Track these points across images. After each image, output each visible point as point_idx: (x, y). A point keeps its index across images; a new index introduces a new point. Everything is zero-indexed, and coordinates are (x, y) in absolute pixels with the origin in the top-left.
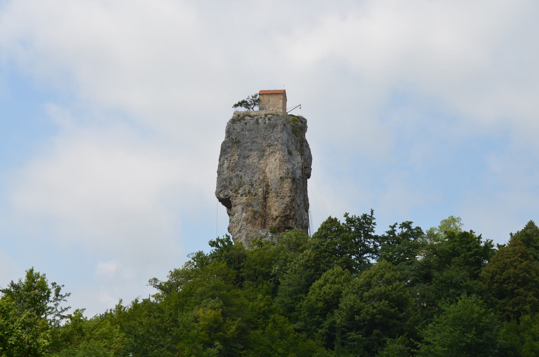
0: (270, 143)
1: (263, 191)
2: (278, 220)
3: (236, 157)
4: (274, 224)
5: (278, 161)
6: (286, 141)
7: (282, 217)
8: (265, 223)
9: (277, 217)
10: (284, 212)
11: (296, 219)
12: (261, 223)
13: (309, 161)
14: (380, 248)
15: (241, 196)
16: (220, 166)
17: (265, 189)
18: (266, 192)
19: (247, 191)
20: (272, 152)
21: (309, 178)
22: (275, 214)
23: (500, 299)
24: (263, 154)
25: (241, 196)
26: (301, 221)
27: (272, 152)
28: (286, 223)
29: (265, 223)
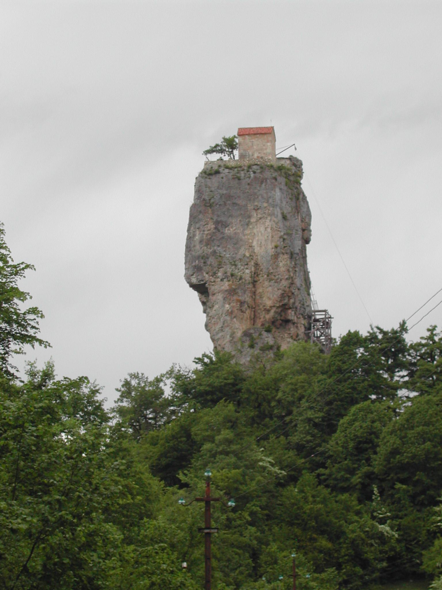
0: (257, 206)
4: (268, 317)
5: (269, 230)
6: (279, 202)
7: (278, 307)
8: (255, 315)
9: (271, 307)
12: (250, 317)
13: (307, 220)
16: (190, 239)
17: (253, 269)
20: (260, 219)
24: (249, 222)
25: (222, 280)
26: (302, 309)
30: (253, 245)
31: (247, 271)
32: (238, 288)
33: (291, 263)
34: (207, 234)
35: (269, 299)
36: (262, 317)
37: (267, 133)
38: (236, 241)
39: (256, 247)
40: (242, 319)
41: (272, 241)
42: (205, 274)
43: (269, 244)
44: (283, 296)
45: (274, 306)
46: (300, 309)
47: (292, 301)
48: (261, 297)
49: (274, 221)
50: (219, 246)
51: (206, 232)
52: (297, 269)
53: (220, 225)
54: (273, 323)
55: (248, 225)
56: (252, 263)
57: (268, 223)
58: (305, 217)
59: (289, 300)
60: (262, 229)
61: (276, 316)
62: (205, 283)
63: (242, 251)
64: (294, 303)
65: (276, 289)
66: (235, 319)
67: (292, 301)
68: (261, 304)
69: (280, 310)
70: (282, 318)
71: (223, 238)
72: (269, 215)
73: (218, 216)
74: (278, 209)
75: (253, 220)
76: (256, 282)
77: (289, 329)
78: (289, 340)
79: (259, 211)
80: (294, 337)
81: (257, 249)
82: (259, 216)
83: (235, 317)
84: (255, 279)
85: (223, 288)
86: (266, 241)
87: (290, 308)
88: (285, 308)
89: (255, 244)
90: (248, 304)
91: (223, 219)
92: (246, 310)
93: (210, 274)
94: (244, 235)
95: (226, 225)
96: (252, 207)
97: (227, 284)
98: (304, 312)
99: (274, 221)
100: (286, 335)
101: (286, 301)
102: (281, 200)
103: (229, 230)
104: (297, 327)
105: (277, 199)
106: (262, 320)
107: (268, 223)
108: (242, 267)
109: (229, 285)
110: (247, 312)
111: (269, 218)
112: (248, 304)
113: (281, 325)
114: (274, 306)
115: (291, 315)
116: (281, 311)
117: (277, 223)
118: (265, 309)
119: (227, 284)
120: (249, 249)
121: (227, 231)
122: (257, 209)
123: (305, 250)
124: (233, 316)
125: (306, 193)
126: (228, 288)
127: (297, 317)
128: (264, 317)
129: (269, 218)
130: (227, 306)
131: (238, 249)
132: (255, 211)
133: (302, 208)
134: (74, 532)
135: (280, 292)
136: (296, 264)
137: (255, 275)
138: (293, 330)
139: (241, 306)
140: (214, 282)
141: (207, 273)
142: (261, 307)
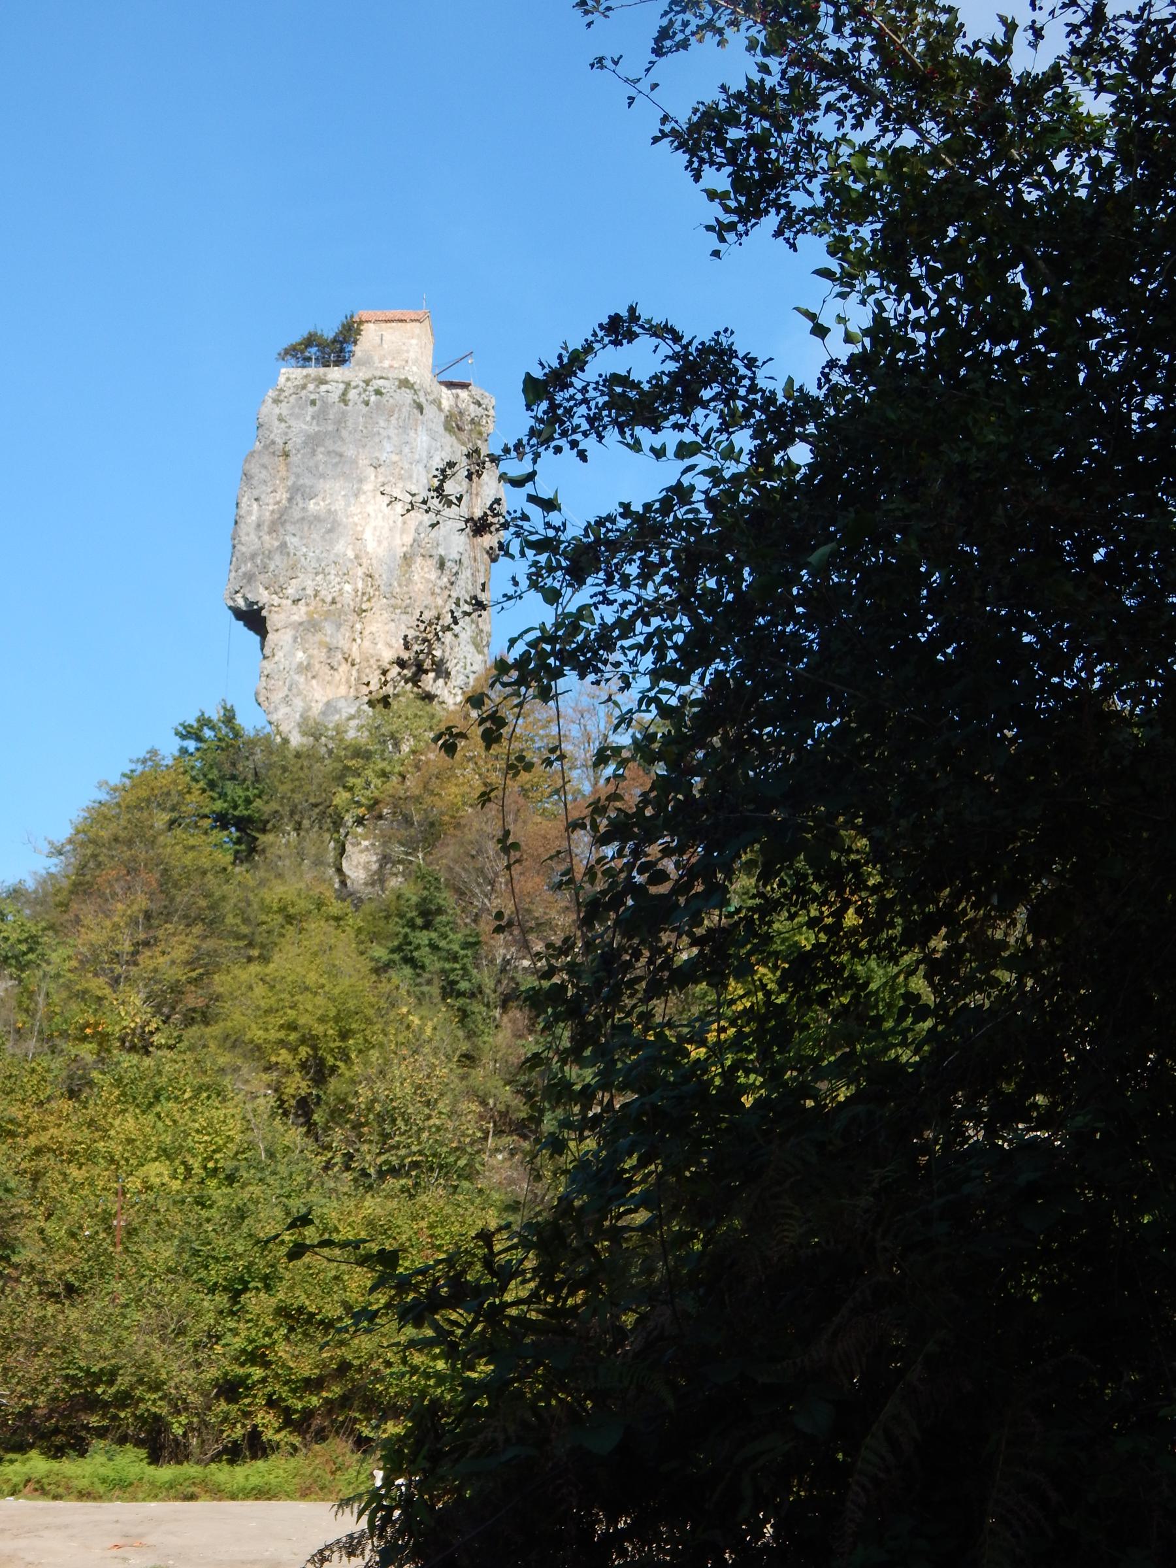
19: (310, 592)
24: (359, 490)
38: (331, 526)
41: (403, 531)
42: (261, 590)
55: (356, 495)
56: (360, 572)
62: (262, 608)
66: (314, 682)
73: (298, 476)
75: (368, 487)
81: (371, 546)
82: (381, 479)
85: (296, 618)
89: (368, 535)
96: (367, 462)
109: (307, 613)
121: (311, 505)
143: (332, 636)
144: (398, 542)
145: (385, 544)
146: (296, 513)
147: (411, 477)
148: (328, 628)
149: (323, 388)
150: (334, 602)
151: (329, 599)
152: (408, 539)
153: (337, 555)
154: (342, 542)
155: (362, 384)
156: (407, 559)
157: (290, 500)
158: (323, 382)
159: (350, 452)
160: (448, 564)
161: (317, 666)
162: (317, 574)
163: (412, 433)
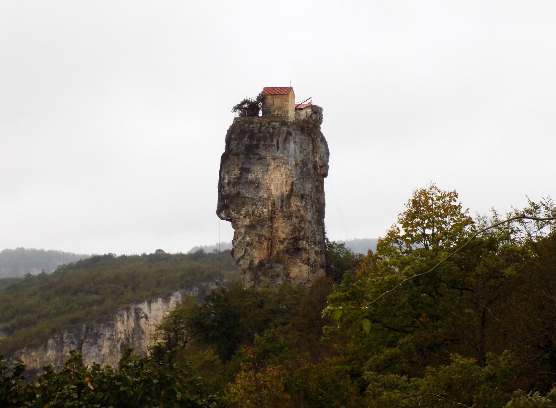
0: (274, 156)
1: (268, 211)
2: (286, 242)
3: (237, 172)
4: (282, 247)
5: (284, 176)
6: (293, 153)
7: (290, 239)
8: (272, 246)
9: (284, 239)
10: (292, 235)
11: (308, 237)
12: (267, 247)
13: (325, 158)
14: (155, 381)
15: (245, 217)
16: (221, 180)
17: (270, 208)
18: (272, 211)
19: (250, 213)
20: (277, 166)
21: (326, 176)
22: (283, 236)
23: (121, 346)
24: (268, 169)
25: (245, 217)
26: (313, 238)
27: (277, 166)
28: (295, 244)
29: (272, 246)
30: (271, 188)
31: (265, 210)
32: (257, 224)
33: (301, 203)
34: (234, 178)
35: (283, 232)
36: (277, 247)
37: (286, 92)
38: (257, 185)
39: (273, 190)
40: (260, 249)
41: (286, 186)
43: (284, 187)
44: (294, 230)
45: (287, 239)
46: (311, 238)
47: (302, 234)
48: (277, 231)
49: (288, 169)
50: (243, 189)
51: (233, 177)
52: (308, 207)
53: (245, 170)
54: (287, 251)
55: (267, 171)
56: (270, 203)
57: (283, 170)
58: (323, 156)
59: (299, 233)
60: (279, 175)
61: (289, 246)
63: (261, 194)
64: (305, 235)
65: (288, 225)
66: (254, 250)
67: (302, 234)
68: (277, 236)
69: (292, 241)
70: (295, 247)
71: (246, 182)
72: (284, 163)
74: (292, 158)
75: (271, 168)
76: (273, 218)
77: (301, 255)
78: (300, 264)
79: (276, 160)
80: (306, 262)
81: (274, 192)
82: (276, 164)
83: (254, 248)
84: (272, 216)
85: (245, 223)
86: (281, 185)
87: (300, 239)
88: (296, 240)
89: (272, 187)
90: (265, 237)
91: (246, 166)
92: (264, 241)
93: (235, 212)
94: (264, 180)
95: (248, 171)
96: (270, 157)
97: (248, 220)
98: (315, 240)
99: (288, 169)
100: (298, 260)
101: (297, 234)
102: (295, 151)
103: (251, 176)
104: (308, 253)
105: (291, 151)
106: (277, 249)
107: (283, 170)
108: (261, 207)
109: (250, 221)
110: (264, 244)
111: (284, 166)
112: (265, 237)
113: (294, 252)
114: (287, 239)
115: (303, 244)
116: (294, 242)
117: (291, 171)
118: (280, 241)
119: (248, 220)
120: (267, 192)
121: (250, 177)
122: (274, 159)
123: (322, 184)
124: (252, 247)
125: (325, 135)
126: (249, 224)
127: (309, 245)
128: (279, 247)
129: (284, 166)
130: (248, 238)
131: (258, 192)
132: (272, 160)
133: (320, 149)
134: (244, 173)
135: (291, 227)
136: (306, 203)
137: (273, 212)
138: (304, 256)
139: (259, 239)
140: (239, 218)
141: (233, 211)
142: (277, 239)
143: (260, 231)
144: (285, 190)
145: (279, 190)
146: (243, 180)
147: (288, 163)
148: (259, 228)
149: (251, 126)
150: (260, 217)
151: (258, 215)
152: (288, 188)
153: (260, 197)
154: (262, 191)
155: (266, 124)
156: (289, 196)
157: (241, 174)
158: (251, 123)
159: (263, 153)
160: (305, 196)
161: (255, 243)
162: (253, 205)
163: (288, 145)
